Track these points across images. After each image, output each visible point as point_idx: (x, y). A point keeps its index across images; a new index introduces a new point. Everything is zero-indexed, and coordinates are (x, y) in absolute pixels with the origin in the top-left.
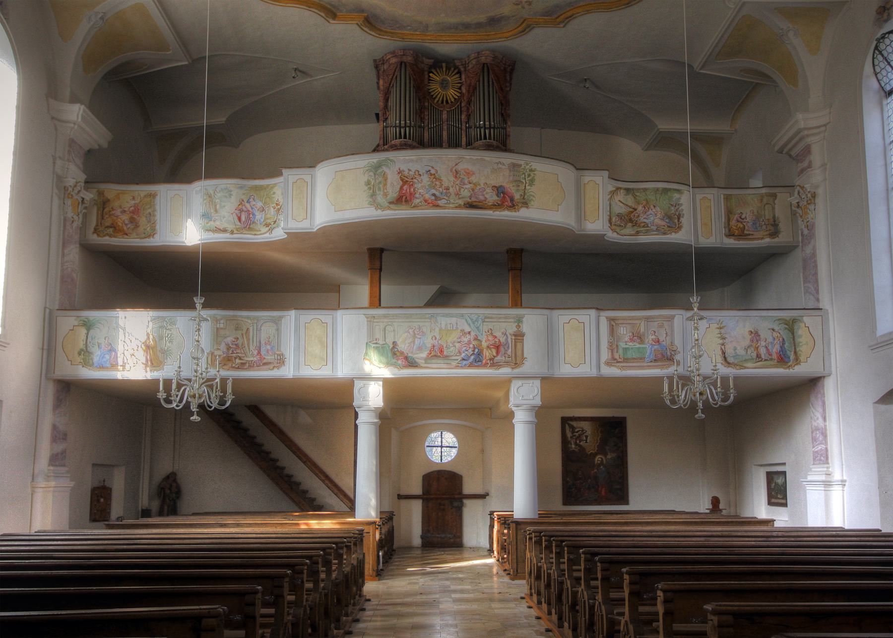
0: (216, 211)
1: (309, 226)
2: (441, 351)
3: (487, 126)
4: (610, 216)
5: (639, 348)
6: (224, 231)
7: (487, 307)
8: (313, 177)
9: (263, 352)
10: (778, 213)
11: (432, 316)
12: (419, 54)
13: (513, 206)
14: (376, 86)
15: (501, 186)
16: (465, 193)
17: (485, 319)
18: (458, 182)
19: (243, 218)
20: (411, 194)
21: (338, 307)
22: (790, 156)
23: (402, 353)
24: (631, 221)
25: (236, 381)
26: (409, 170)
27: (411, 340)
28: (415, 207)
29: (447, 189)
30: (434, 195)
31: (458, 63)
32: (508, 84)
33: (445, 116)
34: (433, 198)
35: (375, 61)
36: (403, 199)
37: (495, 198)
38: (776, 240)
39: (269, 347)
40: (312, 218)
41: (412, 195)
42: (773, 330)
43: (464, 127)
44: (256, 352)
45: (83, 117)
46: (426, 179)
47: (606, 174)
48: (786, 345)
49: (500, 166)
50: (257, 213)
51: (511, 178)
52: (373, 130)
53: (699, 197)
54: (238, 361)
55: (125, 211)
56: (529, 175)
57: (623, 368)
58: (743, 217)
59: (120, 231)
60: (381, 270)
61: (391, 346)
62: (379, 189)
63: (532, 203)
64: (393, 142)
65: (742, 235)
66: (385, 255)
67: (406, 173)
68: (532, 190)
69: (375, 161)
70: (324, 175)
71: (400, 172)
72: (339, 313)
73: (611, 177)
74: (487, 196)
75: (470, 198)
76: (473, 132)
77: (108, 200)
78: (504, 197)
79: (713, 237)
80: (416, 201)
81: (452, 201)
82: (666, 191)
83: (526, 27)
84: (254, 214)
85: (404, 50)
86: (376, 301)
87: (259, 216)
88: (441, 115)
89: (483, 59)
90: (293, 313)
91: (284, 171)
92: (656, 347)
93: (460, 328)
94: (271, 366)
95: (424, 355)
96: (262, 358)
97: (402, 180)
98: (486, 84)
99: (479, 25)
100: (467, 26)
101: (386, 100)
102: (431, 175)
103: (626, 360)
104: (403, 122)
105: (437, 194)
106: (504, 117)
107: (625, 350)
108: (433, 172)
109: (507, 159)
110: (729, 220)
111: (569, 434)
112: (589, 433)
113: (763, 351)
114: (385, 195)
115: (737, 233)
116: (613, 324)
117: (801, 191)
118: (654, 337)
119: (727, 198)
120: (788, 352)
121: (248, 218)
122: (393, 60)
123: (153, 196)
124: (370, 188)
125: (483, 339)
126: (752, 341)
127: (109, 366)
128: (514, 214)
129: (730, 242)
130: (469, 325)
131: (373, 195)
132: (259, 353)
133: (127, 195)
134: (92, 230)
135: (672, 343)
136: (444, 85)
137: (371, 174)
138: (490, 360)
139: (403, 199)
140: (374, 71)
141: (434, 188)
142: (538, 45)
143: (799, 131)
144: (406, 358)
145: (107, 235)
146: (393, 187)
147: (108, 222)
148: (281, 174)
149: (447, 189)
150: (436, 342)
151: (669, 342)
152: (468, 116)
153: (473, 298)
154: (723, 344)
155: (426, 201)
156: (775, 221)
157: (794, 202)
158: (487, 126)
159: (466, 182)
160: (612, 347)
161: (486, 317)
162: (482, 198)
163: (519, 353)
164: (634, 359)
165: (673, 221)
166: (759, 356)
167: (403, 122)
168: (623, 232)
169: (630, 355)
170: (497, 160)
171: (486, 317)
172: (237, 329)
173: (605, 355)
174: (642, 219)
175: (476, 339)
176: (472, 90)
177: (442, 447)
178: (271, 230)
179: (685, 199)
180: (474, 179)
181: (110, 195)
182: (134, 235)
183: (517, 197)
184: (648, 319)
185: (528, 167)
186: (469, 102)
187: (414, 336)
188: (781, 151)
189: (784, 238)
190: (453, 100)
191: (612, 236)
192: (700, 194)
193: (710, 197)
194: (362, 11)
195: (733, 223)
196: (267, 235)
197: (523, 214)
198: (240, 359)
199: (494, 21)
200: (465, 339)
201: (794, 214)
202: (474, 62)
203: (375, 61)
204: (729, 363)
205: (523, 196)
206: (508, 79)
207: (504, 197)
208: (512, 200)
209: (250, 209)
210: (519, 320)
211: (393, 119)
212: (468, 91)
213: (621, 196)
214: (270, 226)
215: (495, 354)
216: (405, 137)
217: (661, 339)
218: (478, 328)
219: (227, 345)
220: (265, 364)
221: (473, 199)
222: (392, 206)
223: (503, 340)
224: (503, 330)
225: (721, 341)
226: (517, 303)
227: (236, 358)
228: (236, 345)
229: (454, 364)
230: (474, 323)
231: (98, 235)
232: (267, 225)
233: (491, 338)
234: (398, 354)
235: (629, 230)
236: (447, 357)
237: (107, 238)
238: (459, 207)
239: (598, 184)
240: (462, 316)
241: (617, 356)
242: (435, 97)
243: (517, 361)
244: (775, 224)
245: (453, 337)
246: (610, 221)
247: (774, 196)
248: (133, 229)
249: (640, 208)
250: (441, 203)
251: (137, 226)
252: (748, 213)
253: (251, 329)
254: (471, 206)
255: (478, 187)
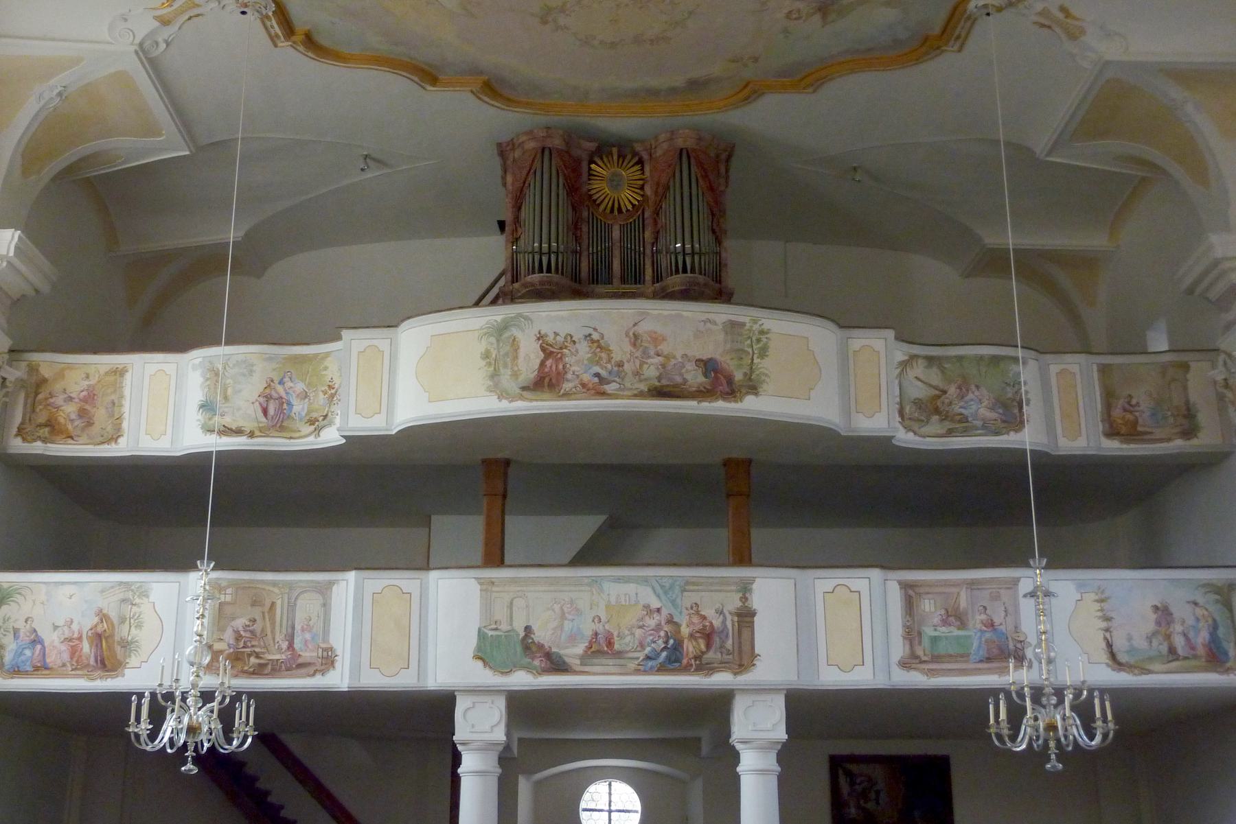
0: (226, 398)
1: (384, 425)
2: (610, 643)
3: (688, 250)
4: (901, 404)
5: (958, 637)
6: (239, 432)
7: (689, 565)
8: (393, 344)
9: (298, 644)
10: (1194, 397)
11: (595, 581)
12: (571, 135)
13: (732, 392)
14: (499, 181)
15: (711, 359)
16: (651, 372)
17: (686, 586)
18: (638, 354)
19: (271, 411)
20: (558, 373)
21: (427, 567)
22: (1207, 299)
23: (540, 646)
24: (937, 411)
25: (264, 700)
26: (556, 334)
27: (555, 624)
28: (567, 395)
29: (620, 365)
30: (597, 375)
31: (638, 147)
32: (722, 181)
33: (616, 233)
34: (596, 380)
35: (499, 145)
36: (545, 382)
37: (701, 379)
38: (1195, 442)
39: (308, 636)
40: (390, 412)
41: (561, 376)
42: (1196, 604)
43: (648, 252)
44: (285, 645)
45: (17, 248)
46: (584, 349)
47: (890, 334)
48: (1221, 632)
49: (709, 325)
50: (294, 401)
51: (728, 346)
52: (489, 253)
53: (1054, 369)
54: (253, 660)
55: (71, 399)
56: (759, 341)
57: (931, 673)
58: (1134, 402)
59: (60, 432)
60: (504, 496)
61: (522, 634)
62: (505, 366)
63: (765, 386)
64: (529, 278)
65: (1131, 433)
66: (512, 471)
67: (550, 339)
68: (764, 365)
69: (499, 318)
70: (414, 337)
71: (540, 337)
72: (433, 575)
73: (899, 338)
74: (688, 377)
75: (659, 379)
76: (664, 262)
77: (44, 381)
78: (716, 378)
79: (1083, 438)
80: (567, 386)
81: (628, 385)
82: (995, 360)
83: (750, 92)
84: (289, 404)
85: (548, 128)
86: (495, 556)
87: (299, 407)
88: (610, 232)
89: (680, 143)
90: (352, 576)
91: (346, 334)
92: (988, 635)
93: (642, 603)
94: (311, 670)
95: (580, 649)
96: (295, 656)
97: (543, 350)
98: (686, 182)
99: (673, 91)
100: (653, 93)
101: (518, 207)
102: (593, 341)
103: (936, 658)
104: (545, 246)
105: (604, 373)
106: (718, 236)
107: (935, 640)
108: (595, 336)
109: (721, 313)
110: (1108, 407)
111: (845, 788)
112: (881, 785)
113: (1179, 642)
114: (515, 375)
115: (1124, 430)
116: (911, 596)
117: (1228, 361)
118: (983, 617)
119: (1104, 370)
120: (1225, 644)
121: (280, 410)
122: (531, 145)
123: (120, 372)
124: (489, 364)
125: (683, 620)
126: (1158, 623)
127: (29, 669)
128: (732, 405)
129: (1113, 447)
130: (658, 596)
131: (494, 376)
132: (291, 646)
133: (79, 371)
134: (15, 430)
135: (1017, 628)
136: (615, 183)
137: (493, 340)
138: (696, 658)
139: (545, 382)
140: (497, 161)
141: (598, 363)
142: (768, 118)
143: (1217, 263)
144: (548, 655)
145: (39, 438)
146: (530, 359)
147: (42, 419)
148: (338, 338)
149: (620, 365)
150: (599, 628)
151: (1011, 627)
152: (657, 234)
153: (665, 537)
154: (1107, 630)
155: (584, 385)
156: (1188, 409)
157: (1220, 378)
158: (688, 250)
159: (652, 353)
160: (912, 634)
161: (687, 583)
162: (678, 379)
163: (746, 648)
164: (951, 658)
165: (1011, 413)
166: (1172, 650)
167: (545, 246)
168: (924, 430)
169: (942, 648)
170: (704, 317)
171: (687, 583)
172: (254, 604)
173: (899, 649)
174: (957, 409)
175: (670, 621)
176: (663, 191)
177: (610, 811)
178: (318, 431)
179: (1028, 373)
180: (665, 348)
181: (45, 372)
182: (84, 439)
183: (738, 376)
184: (972, 585)
185: (756, 327)
186: (657, 213)
187: (563, 616)
188: (1190, 291)
189: (1207, 439)
190: (630, 207)
191: (905, 438)
192: (1055, 365)
193: (1075, 368)
194: (481, 73)
195: (1117, 413)
196: (311, 438)
197: (750, 406)
198: (258, 656)
199: (695, 86)
200: (651, 622)
201: (1221, 398)
202: (665, 146)
203: (499, 145)
204: (1120, 664)
205: (748, 377)
206: (723, 170)
207: (716, 378)
208: (730, 380)
209: (283, 394)
210: (745, 589)
211: (530, 241)
212: (656, 193)
213: (919, 369)
214: (317, 423)
215: (703, 647)
216: (549, 271)
217: (997, 621)
218: (673, 602)
219: (237, 632)
220: (300, 666)
221: (664, 382)
222: (525, 393)
223: (717, 623)
224: (718, 606)
225: (1104, 625)
226: (742, 557)
227: (249, 655)
228: (252, 632)
229: (632, 665)
230: (666, 593)
231: (24, 440)
232: (312, 422)
233: (696, 620)
234: (534, 649)
235: (935, 426)
236: (619, 654)
237: (39, 443)
238: (640, 395)
239: (878, 348)
240: (645, 580)
241: (920, 653)
242: (594, 211)
243: (743, 659)
244: (1189, 414)
245: (631, 618)
246: (901, 413)
247: (1185, 367)
248: (83, 429)
249: (952, 390)
250: (609, 388)
251: (90, 424)
252: (1143, 398)
253: (279, 603)
254: (660, 393)
255: (673, 361)
